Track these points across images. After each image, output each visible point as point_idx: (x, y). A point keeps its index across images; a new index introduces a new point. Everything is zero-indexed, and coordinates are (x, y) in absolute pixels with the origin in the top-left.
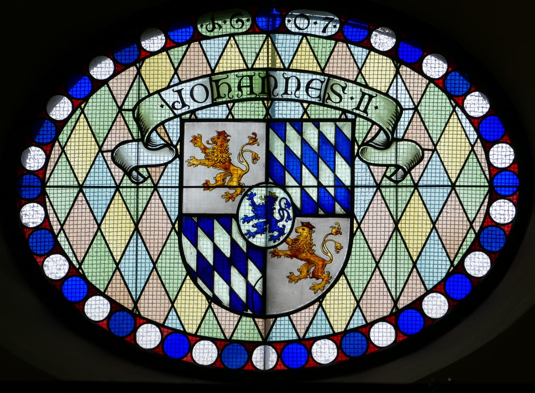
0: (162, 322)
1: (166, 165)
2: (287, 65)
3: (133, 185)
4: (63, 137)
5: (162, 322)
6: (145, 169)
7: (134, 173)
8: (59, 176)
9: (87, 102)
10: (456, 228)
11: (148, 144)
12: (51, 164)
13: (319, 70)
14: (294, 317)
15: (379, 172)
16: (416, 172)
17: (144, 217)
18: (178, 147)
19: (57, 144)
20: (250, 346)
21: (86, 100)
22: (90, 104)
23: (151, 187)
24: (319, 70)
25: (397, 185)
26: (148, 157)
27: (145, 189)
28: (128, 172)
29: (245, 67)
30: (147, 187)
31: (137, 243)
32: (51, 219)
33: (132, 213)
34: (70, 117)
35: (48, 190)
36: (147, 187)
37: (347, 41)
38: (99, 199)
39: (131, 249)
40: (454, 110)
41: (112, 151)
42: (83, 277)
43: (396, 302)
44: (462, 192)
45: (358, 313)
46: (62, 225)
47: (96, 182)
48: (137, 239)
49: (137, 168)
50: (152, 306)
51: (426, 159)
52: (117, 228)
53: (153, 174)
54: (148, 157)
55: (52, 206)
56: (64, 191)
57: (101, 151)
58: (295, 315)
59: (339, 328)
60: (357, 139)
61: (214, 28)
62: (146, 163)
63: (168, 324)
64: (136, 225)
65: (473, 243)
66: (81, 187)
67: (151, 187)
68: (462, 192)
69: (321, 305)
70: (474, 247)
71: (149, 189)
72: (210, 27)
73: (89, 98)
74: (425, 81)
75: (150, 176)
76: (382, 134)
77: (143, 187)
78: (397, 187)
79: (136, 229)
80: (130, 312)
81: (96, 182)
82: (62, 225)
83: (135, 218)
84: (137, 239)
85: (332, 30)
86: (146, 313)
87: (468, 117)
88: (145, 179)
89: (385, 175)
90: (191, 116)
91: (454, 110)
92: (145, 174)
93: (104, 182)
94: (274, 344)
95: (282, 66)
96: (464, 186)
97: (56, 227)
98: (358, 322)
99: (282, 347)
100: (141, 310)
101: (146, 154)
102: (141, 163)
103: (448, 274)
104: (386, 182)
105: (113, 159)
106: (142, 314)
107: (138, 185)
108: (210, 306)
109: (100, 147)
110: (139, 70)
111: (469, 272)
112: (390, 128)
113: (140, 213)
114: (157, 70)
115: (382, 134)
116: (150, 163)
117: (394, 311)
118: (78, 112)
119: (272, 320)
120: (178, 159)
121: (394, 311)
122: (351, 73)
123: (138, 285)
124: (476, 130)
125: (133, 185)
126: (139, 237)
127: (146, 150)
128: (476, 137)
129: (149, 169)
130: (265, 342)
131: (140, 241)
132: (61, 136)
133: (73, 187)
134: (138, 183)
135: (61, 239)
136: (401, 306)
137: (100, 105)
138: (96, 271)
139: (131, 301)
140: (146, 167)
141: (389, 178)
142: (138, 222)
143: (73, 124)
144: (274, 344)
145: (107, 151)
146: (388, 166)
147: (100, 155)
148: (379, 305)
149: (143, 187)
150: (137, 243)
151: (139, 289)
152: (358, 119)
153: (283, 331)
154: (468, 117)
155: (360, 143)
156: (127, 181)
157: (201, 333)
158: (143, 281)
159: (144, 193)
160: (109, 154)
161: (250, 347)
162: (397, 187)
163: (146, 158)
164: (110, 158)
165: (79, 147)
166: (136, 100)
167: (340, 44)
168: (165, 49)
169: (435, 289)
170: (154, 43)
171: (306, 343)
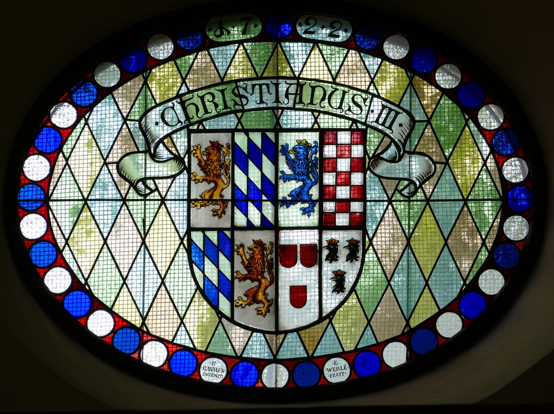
0: (171, 338)
1: (174, 177)
2: (297, 74)
3: (140, 198)
4: (66, 149)
5: (171, 338)
6: (152, 181)
7: (140, 185)
8: (63, 189)
9: (91, 111)
10: (474, 245)
11: (154, 157)
12: (55, 176)
13: (331, 80)
14: (302, 333)
15: (391, 186)
16: (428, 188)
17: (151, 231)
18: (186, 160)
19: (61, 155)
20: (260, 364)
21: (90, 108)
22: (94, 113)
23: (158, 200)
24: (331, 80)
25: (408, 199)
26: (154, 169)
27: (152, 202)
28: (133, 185)
29: (254, 76)
30: (154, 200)
31: (144, 258)
32: (55, 232)
33: (139, 228)
34: (74, 126)
35: (51, 203)
36: (154, 200)
37: (360, 50)
38: (103, 211)
39: (139, 265)
40: (86, 280)
41: (118, 163)
42: (89, 293)
43: (408, 321)
44: (76, 194)
45: (369, 332)
46: (67, 240)
47: (63, 195)
48: (144, 254)
49: (144, 180)
50: (161, 324)
51: (438, 174)
52: (125, 241)
53: (160, 186)
54: (154, 169)
55: (56, 219)
56: (106, 204)
57: (106, 164)
58: (303, 331)
59: (349, 346)
60: (184, 251)
61: (222, 34)
62: (152, 175)
63: (178, 341)
64: (144, 240)
65: (487, 260)
66: (465, 201)
67: (158, 200)
68: (76, 194)
69: (330, 322)
70: (487, 266)
71: (156, 202)
72: (218, 33)
73: (94, 106)
74: (116, 310)
75: (157, 189)
76: (393, 147)
77: (150, 200)
78: (145, 200)
79: (144, 243)
80: (138, 330)
81: (63, 195)
82: (67, 240)
83: (142, 232)
84: (144, 254)
85: (343, 36)
86: (154, 330)
87: (481, 130)
88: (152, 191)
89: (396, 189)
90: (198, 127)
91: (86, 280)
92: (153, 187)
93: (68, 195)
94: (284, 362)
95: (292, 74)
96: (70, 200)
97: (61, 242)
98: (368, 340)
99: (291, 364)
100: (149, 326)
101: (153, 165)
102: (148, 175)
103: (461, 293)
104: (398, 196)
105: (119, 172)
106: (150, 330)
107: (145, 198)
108: (220, 321)
109: (105, 160)
110: (408, 324)
111: (484, 290)
112: (403, 141)
113: (147, 228)
114: (164, 80)
115: (393, 147)
116: (157, 174)
117: (406, 331)
118: (83, 121)
119: (282, 336)
120: (185, 171)
121: (406, 331)
122: (363, 83)
123: (146, 302)
124: (490, 144)
125: (140, 198)
126: (147, 252)
127: (152, 162)
128: (64, 253)
129: (157, 181)
130: (275, 360)
131: (147, 256)
132: (65, 147)
133: (116, 200)
134: (145, 195)
135: (67, 254)
136: (414, 323)
137: (105, 115)
138: (103, 287)
139: (138, 318)
140: (153, 179)
141: (400, 192)
142: (146, 235)
143: (78, 134)
144: (284, 362)
145: (112, 163)
146: (400, 179)
147: (105, 168)
148: (389, 322)
149: (150, 200)
150: (144, 258)
151: (146, 306)
152: (369, 130)
153: (293, 349)
154: (481, 130)
155: (371, 155)
156: (132, 194)
157: (210, 350)
158: (151, 298)
159: (152, 206)
160: (115, 166)
161: (260, 364)
162: (145, 200)
163: (153, 169)
164: (115, 171)
165: (82, 159)
166: (142, 111)
167: (352, 52)
168: (173, 58)
169: (447, 309)
170: (163, 50)
171: (316, 363)
